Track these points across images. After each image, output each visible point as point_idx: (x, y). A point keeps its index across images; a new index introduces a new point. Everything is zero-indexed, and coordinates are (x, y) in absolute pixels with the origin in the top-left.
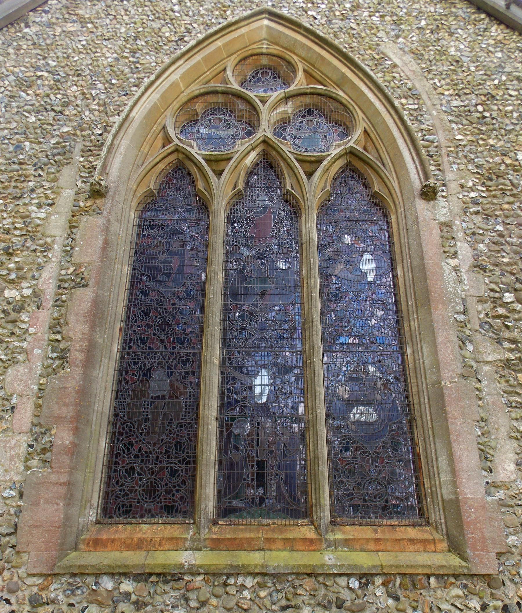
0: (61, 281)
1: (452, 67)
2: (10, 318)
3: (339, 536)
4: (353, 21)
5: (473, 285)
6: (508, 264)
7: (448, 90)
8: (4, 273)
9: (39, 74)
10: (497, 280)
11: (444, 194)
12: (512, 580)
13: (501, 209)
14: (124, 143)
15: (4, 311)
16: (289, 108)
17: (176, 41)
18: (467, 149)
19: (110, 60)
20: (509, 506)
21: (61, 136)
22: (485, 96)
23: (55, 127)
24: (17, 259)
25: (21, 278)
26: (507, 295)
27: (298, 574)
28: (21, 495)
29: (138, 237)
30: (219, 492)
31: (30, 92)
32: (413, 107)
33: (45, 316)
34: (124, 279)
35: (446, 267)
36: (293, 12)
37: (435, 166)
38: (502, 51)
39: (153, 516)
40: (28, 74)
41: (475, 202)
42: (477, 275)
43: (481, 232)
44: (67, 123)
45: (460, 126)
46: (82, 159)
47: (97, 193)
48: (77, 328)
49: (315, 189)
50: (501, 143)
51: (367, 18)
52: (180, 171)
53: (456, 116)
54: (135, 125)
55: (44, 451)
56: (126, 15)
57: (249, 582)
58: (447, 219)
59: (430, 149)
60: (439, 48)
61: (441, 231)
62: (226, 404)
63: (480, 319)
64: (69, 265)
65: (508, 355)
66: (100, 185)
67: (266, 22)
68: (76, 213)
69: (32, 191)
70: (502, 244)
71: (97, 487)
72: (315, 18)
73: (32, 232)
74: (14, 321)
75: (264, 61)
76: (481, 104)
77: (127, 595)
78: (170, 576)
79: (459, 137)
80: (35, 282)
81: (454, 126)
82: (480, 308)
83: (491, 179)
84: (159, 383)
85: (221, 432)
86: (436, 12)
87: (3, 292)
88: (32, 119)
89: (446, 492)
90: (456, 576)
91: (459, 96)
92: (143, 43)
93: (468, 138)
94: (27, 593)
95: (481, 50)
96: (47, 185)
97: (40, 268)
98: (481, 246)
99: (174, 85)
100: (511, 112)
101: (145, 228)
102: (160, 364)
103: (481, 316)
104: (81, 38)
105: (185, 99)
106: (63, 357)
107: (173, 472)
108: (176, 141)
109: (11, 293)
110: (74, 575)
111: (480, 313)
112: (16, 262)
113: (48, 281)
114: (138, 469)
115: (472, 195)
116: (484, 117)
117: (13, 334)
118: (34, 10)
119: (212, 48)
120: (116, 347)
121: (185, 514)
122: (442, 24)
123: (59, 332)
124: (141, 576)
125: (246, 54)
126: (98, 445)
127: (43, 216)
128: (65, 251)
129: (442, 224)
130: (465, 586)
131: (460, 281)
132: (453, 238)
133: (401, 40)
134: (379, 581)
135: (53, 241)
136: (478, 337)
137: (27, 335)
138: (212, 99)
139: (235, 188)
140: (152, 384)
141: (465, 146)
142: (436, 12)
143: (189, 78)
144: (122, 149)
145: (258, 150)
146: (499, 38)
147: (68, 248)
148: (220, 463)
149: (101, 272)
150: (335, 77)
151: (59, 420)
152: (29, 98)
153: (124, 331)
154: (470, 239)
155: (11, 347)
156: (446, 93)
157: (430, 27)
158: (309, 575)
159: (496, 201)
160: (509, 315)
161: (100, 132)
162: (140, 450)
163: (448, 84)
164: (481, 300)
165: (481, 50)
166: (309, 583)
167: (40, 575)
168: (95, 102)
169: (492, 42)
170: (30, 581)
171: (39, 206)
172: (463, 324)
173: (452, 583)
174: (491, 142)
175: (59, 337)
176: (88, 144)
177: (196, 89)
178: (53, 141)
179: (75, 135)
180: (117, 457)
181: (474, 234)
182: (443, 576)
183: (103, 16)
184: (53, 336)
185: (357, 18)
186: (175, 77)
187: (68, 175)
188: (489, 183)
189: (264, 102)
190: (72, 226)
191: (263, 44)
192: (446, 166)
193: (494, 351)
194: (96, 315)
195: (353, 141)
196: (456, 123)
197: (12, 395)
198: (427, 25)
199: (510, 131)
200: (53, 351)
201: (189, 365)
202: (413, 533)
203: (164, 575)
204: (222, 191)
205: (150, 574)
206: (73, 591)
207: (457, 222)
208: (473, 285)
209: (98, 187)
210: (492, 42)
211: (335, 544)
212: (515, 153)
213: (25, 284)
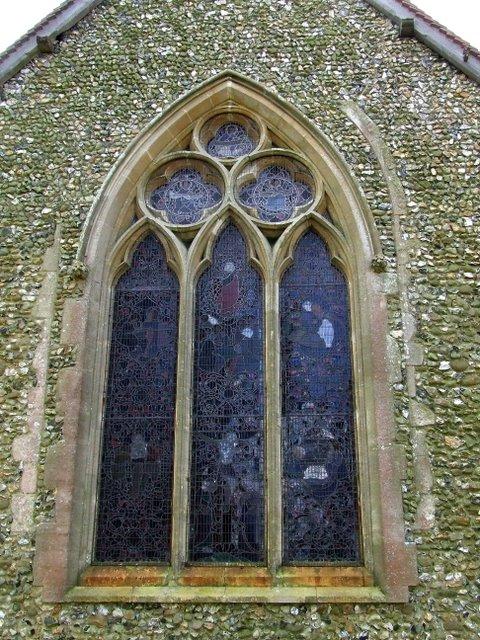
0: (52, 360)
1: (410, 126)
2: (11, 395)
3: (287, 575)
4: (315, 76)
5: (414, 354)
6: (447, 333)
7: (404, 152)
8: (4, 353)
9: (19, 152)
10: (436, 349)
11: (393, 265)
12: (421, 608)
13: (447, 278)
14: (101, 223)
15: (6, 389)
16: (253, 171)
17: (144, 109)
18: (418, 216)
19: (83, 133)
20: (425, 550)
21: (42, 219)
22: (439, 158)
23: (37, 209)
24: (14, 340)
25: (19, 358)
26: (443, 363)
27: (250, 604)
28: (33, 543)
29: (115, 310)
30: (191, 541)
31: (12, 172)
32: (369, 172)
33: (40, 393)
34: (105, 353)
35: (388, 337)
36: (256, 68)
37: (388, 235)
38: (459, 106)
39: (137, 560)
40: (9, 153)
41: (422, 271)
42: (418, 345)
43: (425, 301)
44: (47, 204)
45: (414, 192)
46: (63, 241)
47: (80, 277)
48: (68, 406)
49: (271, 258)
50: (451, 209)
51: (329, 73)
52: (148, 248)
53: (410, 181)
54: (109, 205)
55: (49, 508)
56: (95, 81)
57: (213, 610)
58: (394, 292)
59: (383, 217)
60: (398, 105)
61: (389, 303)
62: (196, 466)
63: (417, 386)
64: (58, 346)
65: (439, 419)
66: (81, 271)
67: (230, 84)
68: (62, 295)
69: (21, 274)
70: (444, 313)
71: (91, 537)
72: (278, 75)
73: (23, 315)
74: (15, 398)
75: (230, 118)
76: (435, 167)
77: (119, 619)
78: (152, 606)
79: (411, 204)
80: (30, 362)
81: (408, 192)
82: (418, 376)
83: (438, 247)
84: (139, 448)
85: (192, 491)
86: (397, 62)
87: (4, 371)
88: (16, 202)
89: (376, 539)
90: (376, 605)
91: (415, 159)
92: (113, 113)
93: (421, 204)
94: (43, 617)
95: (440, 105)
96: (34, 268)
97: (33, 348)
98: (425, 316)
99: (145, 156)
100: (463, 175)
101: (120, 299)
102: (139, 430)
103: (419, 384)
104: (54, 110)
105: (155, 168)
106: (58, 427)
107: (152, 524)
108: (148, 215)
109: (10, 372)
110: (79, 604)
111: (417, 381)
112: (12, 343)
113: (40, 362)
114: (123, 521)
115: (421, 264)
116: (437, 181)
117: (15, 408)
118: (9, 82)
119: (179, 116)
120: (100, 417)
121: (163, 559)
122: (404, 76)
123: (54, 407)
124: (127, 605)
125: (212, 115)
126: (90, 502)
127: (32, 299)
128: (54, 333)
129: (389, 296)
130: (383, 612)
131: (403, 352)
132: (399, 310)
133: (361, 97)
134: (314, 609)
135: (43, 323)
136: (414, 404)
137: (26, 410)
138: (180, 164)
139: (202, 258)
140: (133, 449)
141: (416, 213)
142: (397, 62)
143: (156, 149)
144: (98, 230)
145: (224, 218)
146: (459, 90)
147: (56, 330)
148: (192, 517)
149: (87, 351)
150: (296, 140)
151: (60, 483)
152: (11, 179)
153: (107, 401)
154: (414, 309)
155: (15, 420)
156: (403, 156)
157: (391, 81)
158: (260, 605)
159: (442, 269)
160: (443, 382)
161: (77, 213)
162: (124, 505)
163: (404, 146)
164: (420, 369)
165: (440, 105)
166: (259, 611)
167: (52, 604)
168: (71, 181)
169: (450, 95)
170: (44, 608)
171: (28, 289)
172: (400, 393)
173: (372, 611)
174: (441, 208)
175: (53, 412)
176: (67, 225)
177: (164, 157)
178: (36, 223)
179: (55, 216)
180: (106, 511)
181: (419, 304)
182: (366, 604)
183: (73, 83)
184: (49, 411)
185: (320, 72)
186: (145, 150)
187: (51, 256)
188: (437, 251)
189: (229, 167)
190: (58, 307)
191: (228, 104)
192: (397, 235)
193: (428, 416)
194: (83, 391)
195: (313, 207)
196: (410, 189)
197: (19, 462)
198: (389, 78)
199: (460, 196)
200: (49, 424)
201: (164, 432)
202: (348, 572)
203: (147, 604)
204: (186, 261)
205: (136, 604)
206: (77, 615)
207: (404, 293)
208: (414, 354)
209: (79, 273)
210: (450, 95)
211: (282, 582)
212: (463, 220)
213: (22, 364)
